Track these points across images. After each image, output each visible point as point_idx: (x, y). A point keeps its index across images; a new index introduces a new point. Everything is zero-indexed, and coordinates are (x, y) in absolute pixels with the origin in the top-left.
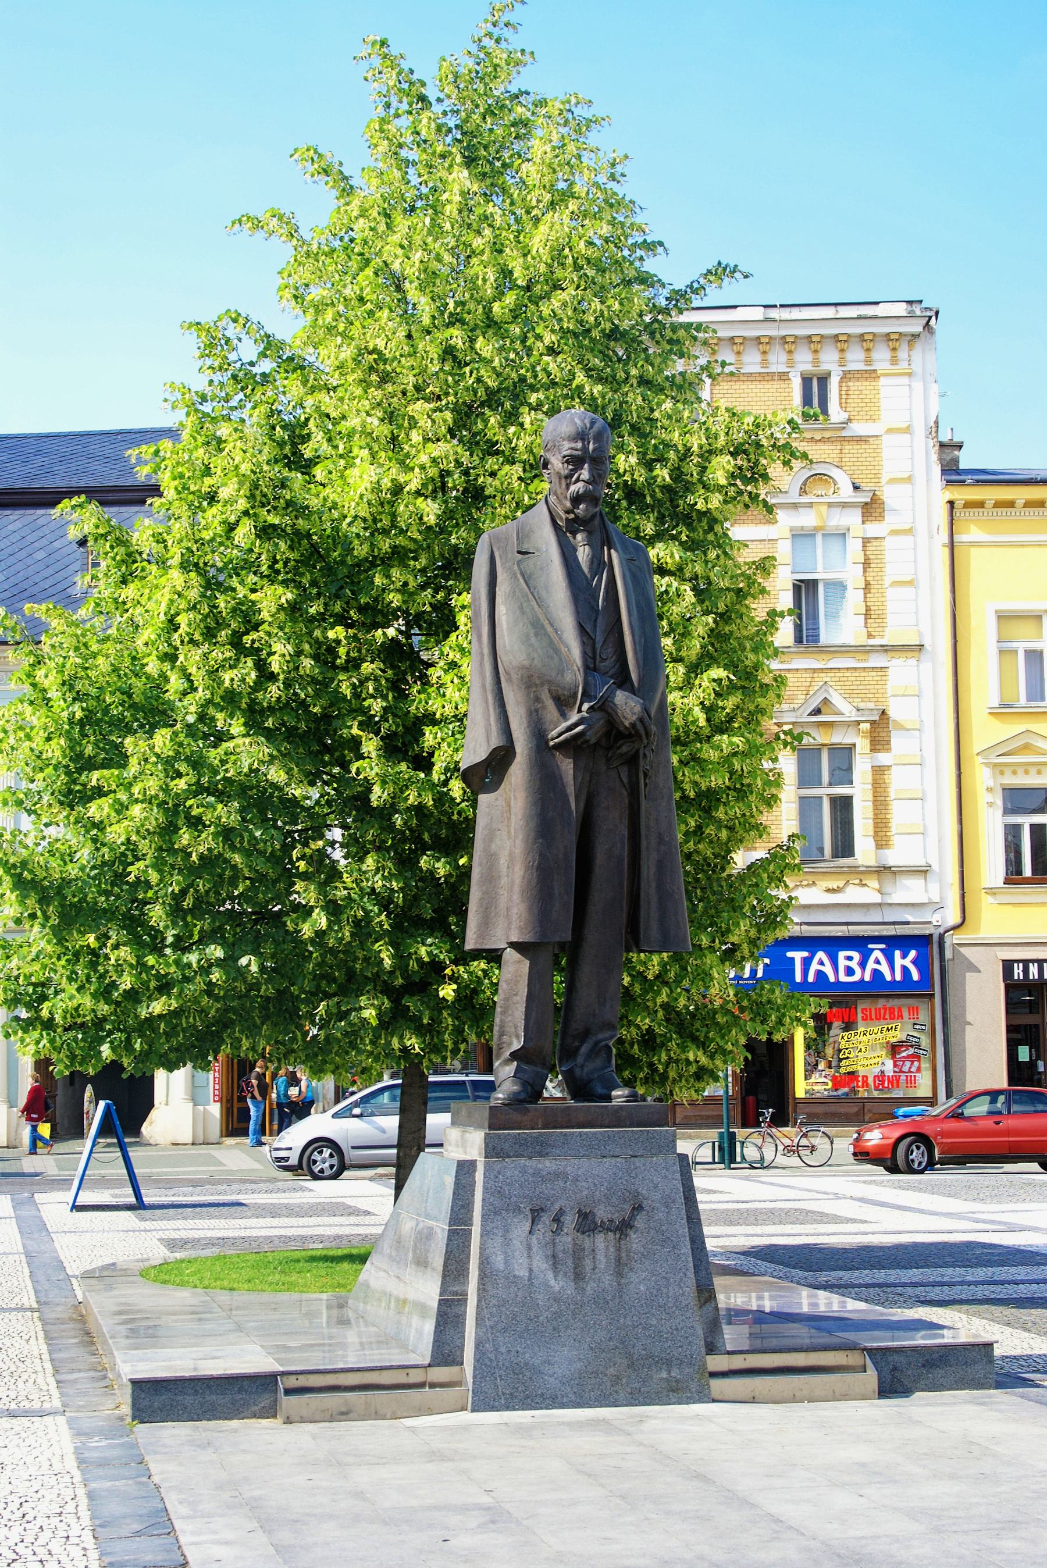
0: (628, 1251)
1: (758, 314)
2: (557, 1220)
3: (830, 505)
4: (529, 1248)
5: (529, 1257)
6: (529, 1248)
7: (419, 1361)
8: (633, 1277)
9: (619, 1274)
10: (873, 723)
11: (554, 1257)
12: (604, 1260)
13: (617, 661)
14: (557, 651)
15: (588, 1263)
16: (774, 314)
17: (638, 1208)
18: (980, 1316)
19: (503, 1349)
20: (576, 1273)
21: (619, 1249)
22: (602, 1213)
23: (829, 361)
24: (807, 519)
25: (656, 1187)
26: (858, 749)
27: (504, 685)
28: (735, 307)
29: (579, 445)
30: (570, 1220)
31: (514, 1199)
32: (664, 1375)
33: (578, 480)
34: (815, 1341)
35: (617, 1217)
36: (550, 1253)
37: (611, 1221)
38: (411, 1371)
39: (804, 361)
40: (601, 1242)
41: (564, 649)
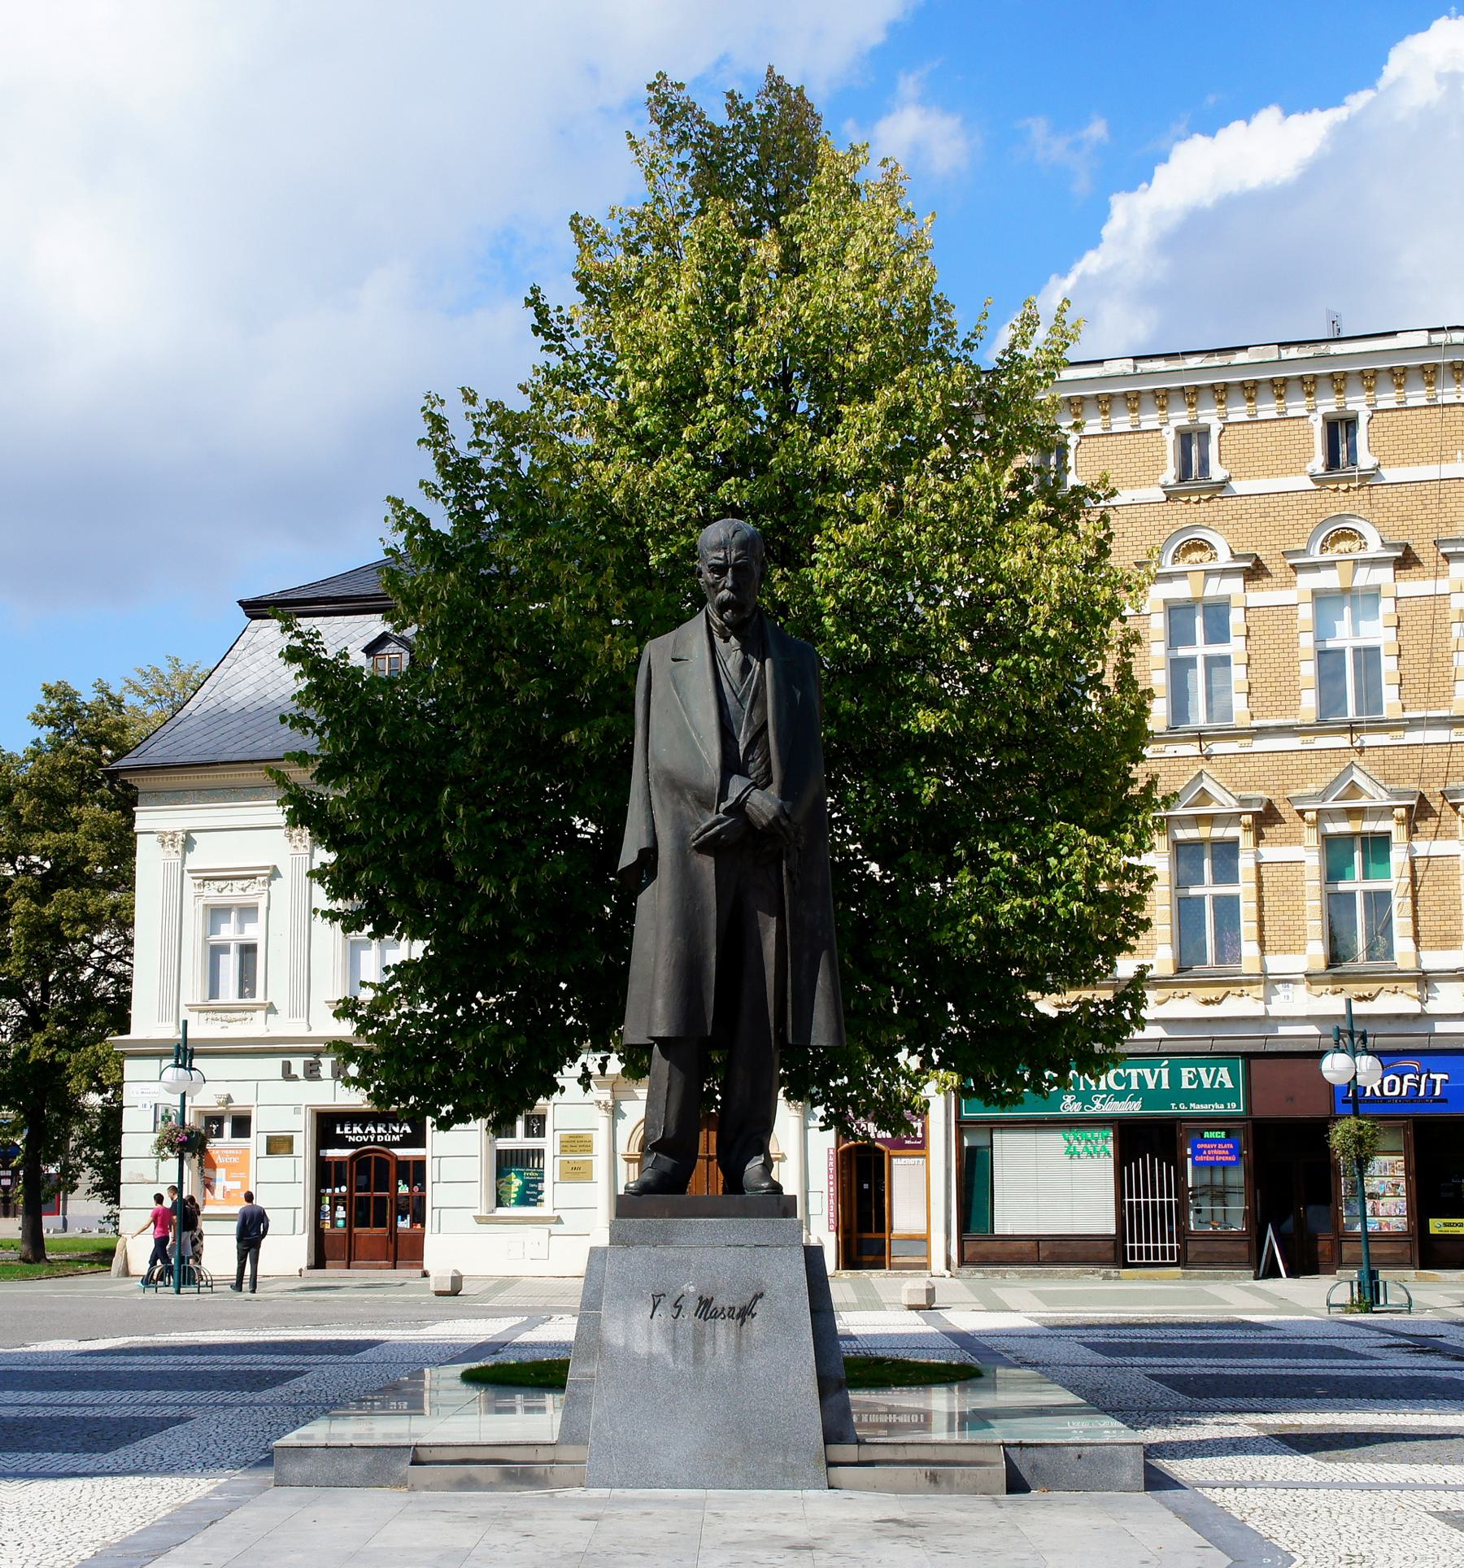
0: (748, 1338)
1: (1421, 339)
2: (677, 1306)
3: (1208, 573)
4: (650, 1333)
5: (650, 1340)
6: (650, 1333)
7: (548, 1440)
8: (752, 1363)
9: (739, 1360)
10: (1409, 808)
11: (674, 1341)
12: (724, 1346)
13: (762, 763)
14: (699, 755)
15: (708, 1348)
16: (1438, 338)
17: (759, 1296)
18: (1359, 1459)
19: (620, 1429)
20: (695, 1358)
21: (739, 1336)
22: (720, 1302)
23: (1357, 403)
24: (1329, 580)
25: (780, 1276)
26: (1394, 839)
27: (652, 789)
28: (1395, 333)
29: (722, 555)
30: (691, 1305)
31: (636, 1285)
32: (780, 1460)
33: (723, 588)
34: (1282, 1500)
35: (738, 1305)
36: (670, 1338)
37: (732, 1309)
38: (540, 1449)
39: (1328, 405)
40: (723, 1329)
41: (704, 754)
